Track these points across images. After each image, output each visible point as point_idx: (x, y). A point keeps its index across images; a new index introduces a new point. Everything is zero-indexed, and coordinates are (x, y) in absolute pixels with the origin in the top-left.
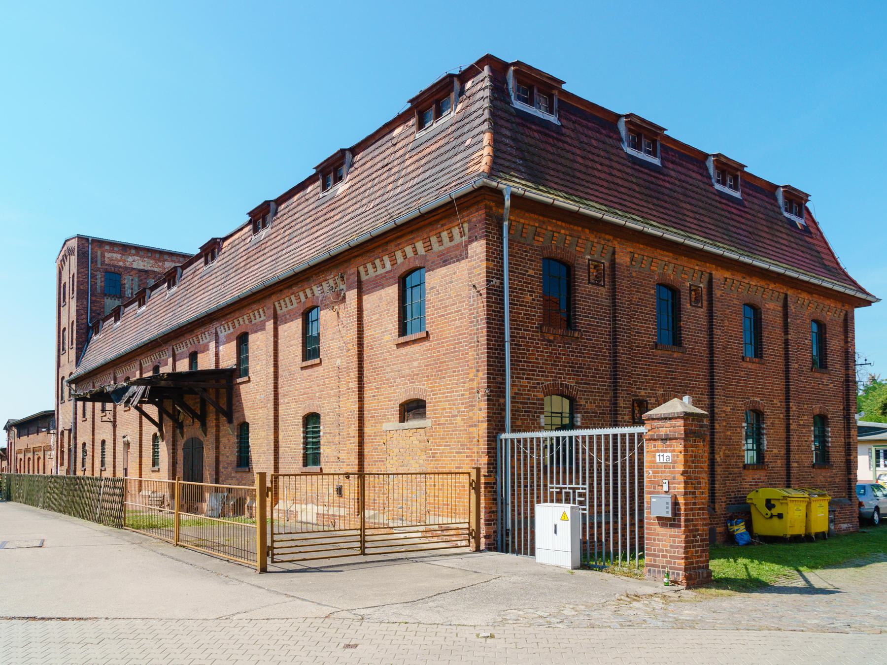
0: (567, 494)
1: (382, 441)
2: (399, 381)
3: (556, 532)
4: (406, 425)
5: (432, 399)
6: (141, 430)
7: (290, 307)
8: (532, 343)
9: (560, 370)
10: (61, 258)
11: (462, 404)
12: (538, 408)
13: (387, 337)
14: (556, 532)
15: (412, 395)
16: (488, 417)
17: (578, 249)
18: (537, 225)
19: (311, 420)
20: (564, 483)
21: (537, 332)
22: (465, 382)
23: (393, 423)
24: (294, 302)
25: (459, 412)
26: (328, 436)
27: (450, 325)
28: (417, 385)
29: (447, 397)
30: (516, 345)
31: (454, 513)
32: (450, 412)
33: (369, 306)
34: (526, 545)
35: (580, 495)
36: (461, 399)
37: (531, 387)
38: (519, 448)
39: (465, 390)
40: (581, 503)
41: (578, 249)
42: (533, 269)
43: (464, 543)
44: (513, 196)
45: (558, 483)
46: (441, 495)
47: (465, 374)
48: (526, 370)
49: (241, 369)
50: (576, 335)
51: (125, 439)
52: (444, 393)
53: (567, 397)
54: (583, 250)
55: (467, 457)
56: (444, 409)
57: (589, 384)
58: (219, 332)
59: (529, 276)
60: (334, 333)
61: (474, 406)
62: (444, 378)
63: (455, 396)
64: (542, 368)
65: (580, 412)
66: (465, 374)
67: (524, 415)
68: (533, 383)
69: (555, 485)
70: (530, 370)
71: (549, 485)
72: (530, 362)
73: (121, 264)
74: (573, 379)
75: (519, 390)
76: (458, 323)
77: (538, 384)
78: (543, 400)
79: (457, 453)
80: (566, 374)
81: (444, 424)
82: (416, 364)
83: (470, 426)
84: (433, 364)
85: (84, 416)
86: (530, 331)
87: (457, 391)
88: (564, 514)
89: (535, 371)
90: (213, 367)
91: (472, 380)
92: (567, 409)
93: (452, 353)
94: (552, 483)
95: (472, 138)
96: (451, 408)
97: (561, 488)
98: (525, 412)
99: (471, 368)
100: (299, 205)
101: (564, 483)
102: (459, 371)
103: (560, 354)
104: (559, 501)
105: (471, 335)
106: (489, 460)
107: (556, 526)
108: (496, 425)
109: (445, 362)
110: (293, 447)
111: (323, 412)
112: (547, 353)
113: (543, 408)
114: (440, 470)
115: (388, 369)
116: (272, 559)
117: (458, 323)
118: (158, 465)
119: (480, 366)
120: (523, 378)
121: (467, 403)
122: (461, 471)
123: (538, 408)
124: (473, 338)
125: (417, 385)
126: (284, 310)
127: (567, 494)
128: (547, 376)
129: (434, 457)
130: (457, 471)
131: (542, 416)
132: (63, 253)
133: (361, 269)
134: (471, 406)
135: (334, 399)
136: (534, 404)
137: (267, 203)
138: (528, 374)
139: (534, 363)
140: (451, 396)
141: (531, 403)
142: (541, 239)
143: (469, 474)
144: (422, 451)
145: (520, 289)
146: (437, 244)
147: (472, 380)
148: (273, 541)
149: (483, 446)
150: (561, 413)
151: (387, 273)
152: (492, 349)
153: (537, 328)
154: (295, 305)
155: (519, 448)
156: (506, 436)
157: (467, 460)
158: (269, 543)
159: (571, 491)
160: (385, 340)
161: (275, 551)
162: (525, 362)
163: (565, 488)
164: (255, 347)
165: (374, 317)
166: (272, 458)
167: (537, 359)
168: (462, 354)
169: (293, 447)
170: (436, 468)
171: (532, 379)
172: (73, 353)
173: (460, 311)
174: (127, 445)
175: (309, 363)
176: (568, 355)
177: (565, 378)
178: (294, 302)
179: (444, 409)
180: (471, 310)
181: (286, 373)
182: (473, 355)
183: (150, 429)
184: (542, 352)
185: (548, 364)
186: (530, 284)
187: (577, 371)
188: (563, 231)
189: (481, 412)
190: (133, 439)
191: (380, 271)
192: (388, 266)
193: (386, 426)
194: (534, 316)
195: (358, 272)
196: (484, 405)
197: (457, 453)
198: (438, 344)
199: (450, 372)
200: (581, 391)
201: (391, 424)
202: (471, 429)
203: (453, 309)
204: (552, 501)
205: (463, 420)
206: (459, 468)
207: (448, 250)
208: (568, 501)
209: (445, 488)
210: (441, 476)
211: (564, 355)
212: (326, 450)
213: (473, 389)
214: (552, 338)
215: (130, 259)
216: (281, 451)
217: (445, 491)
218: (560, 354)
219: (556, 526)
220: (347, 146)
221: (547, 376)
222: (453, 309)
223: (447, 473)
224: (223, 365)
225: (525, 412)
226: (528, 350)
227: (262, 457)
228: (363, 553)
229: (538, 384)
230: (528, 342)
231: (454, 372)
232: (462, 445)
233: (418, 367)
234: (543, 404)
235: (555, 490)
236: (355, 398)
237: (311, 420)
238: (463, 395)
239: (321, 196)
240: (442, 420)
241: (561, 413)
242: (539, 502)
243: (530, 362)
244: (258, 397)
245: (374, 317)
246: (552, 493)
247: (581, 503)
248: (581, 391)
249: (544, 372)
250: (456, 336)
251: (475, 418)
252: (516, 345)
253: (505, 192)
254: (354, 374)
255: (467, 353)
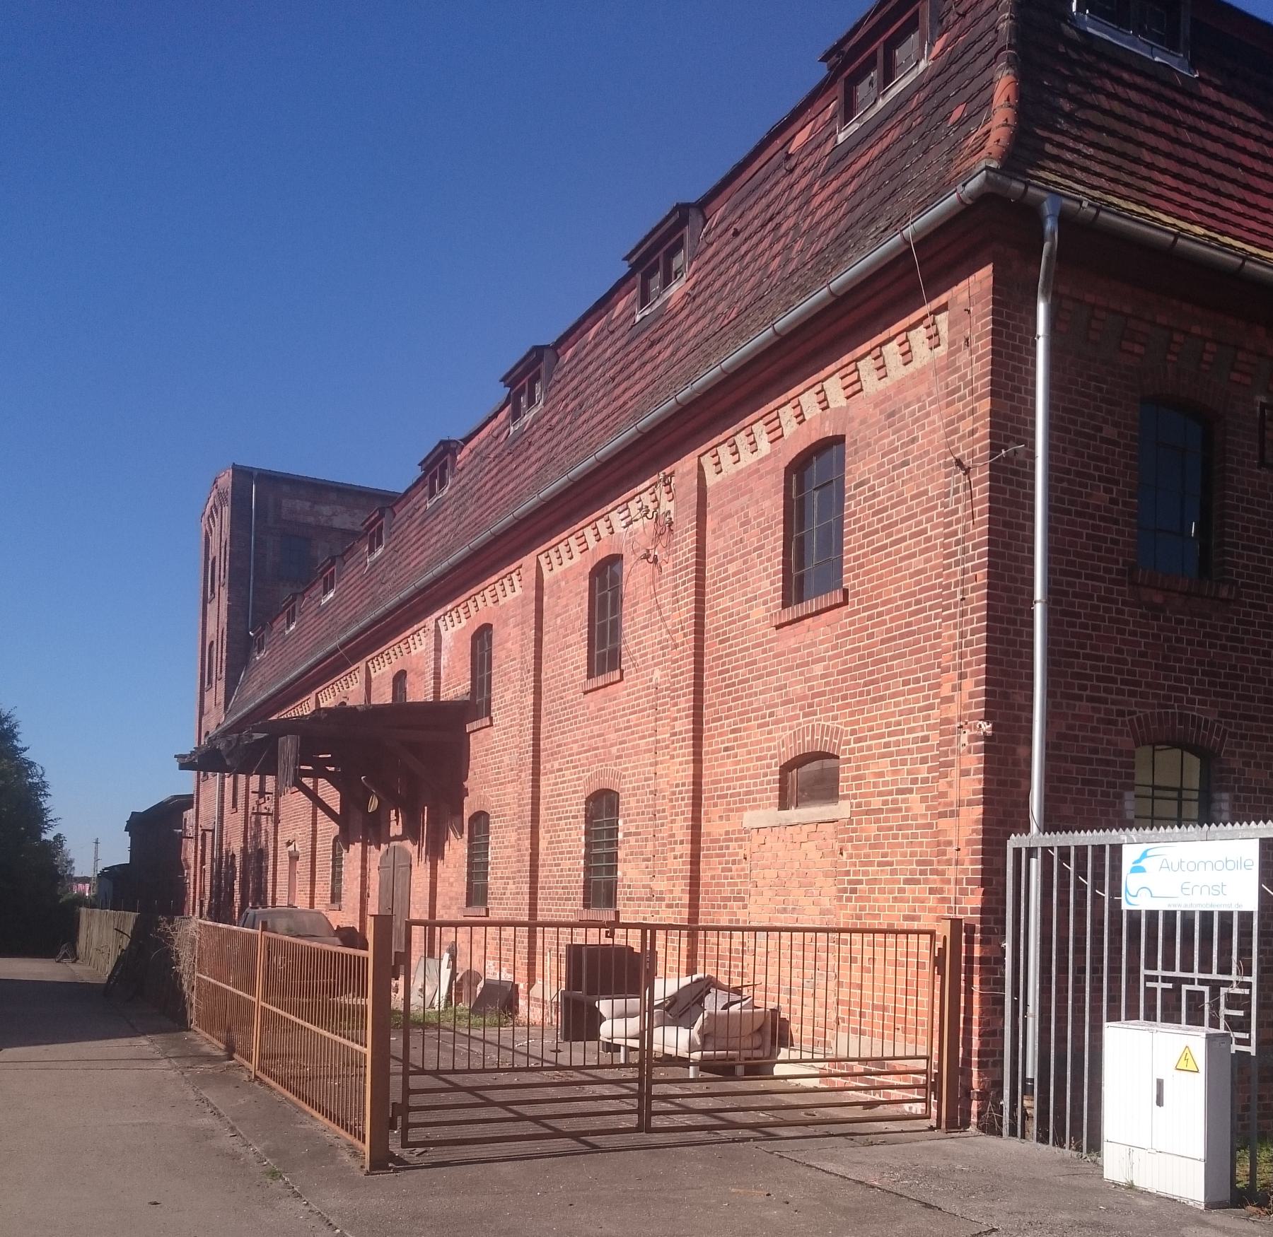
0: (1195, 998)
1: (741, 852)
2: (780, 711)
3: (1160, 1102)
4: (794, 814)
5: (852, 751)
6: (314, 831)
7: (568, 563)
8: (1107, 610)
9: (1178, 679)
10: (208, 512)
11: (924, 760)
12: (1117, 775)
13: (758, 612)
14: (1160, 1102)
15: (806, 744)
16: (985, 791)
17: (1235, 376)
18: (1127, 309)
19: (602, 807)
20: (1187, 967)
21: (1121, 583)
22: (931, 707)
23: (764, 814)
24: (576, 550)
25: (914, 781)
26: (632, 839)
27: (898, 570)
28: (820, 720)
29: (887, 745)
30: (1065, 613)
31: (899, 1025)
32: (894, 782)
33: (721, 543)
34: (1077, 1119)
35: (1233, 1001)
36: (920, 750)
37: (1100, 720)
38: (1064, 874)
39: (930, 727)
40: (1235, 1024)
41: (1235, 376)
42: (1116, 425)
43: (918, 1108)
44: (1065, 219)
45: (1169, 965)
46: (867, 983)
47: (931, 688)
48: (1089, 678)
49: (476, 706)
50: (1224, 593)
51: (291, 848)
52: (882, 736)
53: (1195, 750)
54: (1248, 381)
55: (932, 891)
56: (881, 775)
57: (1253, 718)
58: (443, 629)
59: (1103, 440)
60: (650, 612)
61: (951, 764)
62: (882, 698)
63: (906, 742)
64: (1130, 673)
65: (1227, 790)
66: (931, 688)
67: (1080, 792)
68: (1108, 712)
69: (1159, 972)
70: (1099, 679)
71: (1143, 972)
72: (1101, 659)
73: (311, 519)
74: (1213, 704)
75: (1071, 727)
76: (917, 563)
77: (1121, 713)
78: (1131, 754)
79: (907, 881)
80: (1195, 692)
81: (880, 811)
82: (818, 669)
83: (942, 815)
84: (857, 668)
85: (235, 805)
86: (1102, 579)
87: (911, 731)
88: (1187, 1053)
89: (1114, 681)
90: (430, 698)
91: (949, 700)
92: (1193, 779)
93: (902, 636)
94: (1151, 965)
95: (968, 101)
96: (895, 772)
97: (1178, 982)
98: (1085, 782)
99: (946, 670)
100: (596, 346)
101: (1187, 967)
102: (917, 681)
103: (1179, 640)
104: (1171, 1016)
105: (948, 587)
106: (984, 902)
107: (1160, 1084)
108: (1002, 811)
109: (884, 660)
110: (566, 864)
111: (625, 788)
112: (1145, 635)
113: (1132, 776)
114: (869, 923)
115: (758, 686)
116: (404, 1136)
117: (917, 563)
118: (340, 899)
119: (968, 664)
120: (1080, 698)
121: (934, 758)
122: (915, 925)
123: (1117, 775)
124: (954, 595)
125: (820, 720)
126: (558, 569)
127: (1195, 998)
128: (1143, 695)
129: (854, 891)
130: (906, 925)
131: (1129, 795)
132: (210, 504)
133: (708, 461)
134: (943, 765)
135: (648, 758)
136: (1108, 763)
137: (538, 351)
138: (1094, 688)
139: (1110, 660)
140: (897, 743)
141: (1100, 761)
142: (1137, 349)
143: (932, 933)
144: (826, 875)
145: (1078, 474)
146: (875, 375)
147: (949, 700)
148: (407, 1092)
149: (971, 866)
150: (1180, 790)
151: (761, 461)
152: (1001, 620)
153: (1120, 572)
154: (578, 557)
155: (1064, 874)
156: (1035, 836)
157: (932, 901)
158: (396, 1096)
159: (1206, 989)
160: (753, 619)
161: (414, 1118)
162: (1087, 657)
163: (1192, 981)
164: (503, 654)
165: (732, 568)
166: (526, 888)
167: (1119, 651)
168: (927, 639)
169: (566, 864)
170: (859, 917)
171: (1105, 701)
172: (221, 686)
173: (924, 531)
174: (294, 858)
175: (600, 681)
176: (1201, 644)
177: (1192, 701)
178: (576, 550)
179: (881, 775)
180: (949, 524)
181: (556, 706)
182: (951, 637)
183: (329, 829)
184: (1133, 633)
185: (1148, 665)
186: (1106, 460)
187: (1223, 685)
188: (1196, 330)
189: (967, 784)
190: (302, 847)
191: (747, 459)
192: (764, 447)
193: (751, 818)
194: (1115, 542)
195: (700, 467)
196: (975, 762)
197: (907, 881)
198: (870, 618)
199: (896, 685)
200: (1233, 735)
201: (761, 812)
202: (944, 823)
203: (905, 530)
204: (1150, 1016)
205: (924, 800)
206: (913, 918)
207: (900, 387)
208: (1195, 1019)
209: (879, 965)
210: (868, 937)
211: (1190, 642)
212: (628, 872)
213: (947, 721)
214: (1158, 599)
215: (326, 510)
216: (542, 873)
217: (879, 975)
218: (1179, 640)
219: (1160, 1084)
220: (693, 198)
221: (1143, 695)
222: (905, 530)
223: (884, 932)
224: (447, 694)
225: (1085, 782)
226: (1095, 628)
227: (511, 886)
228: (644, 1127)
229: (1121, 713)
230: (1096, 608)
231: (906, 683)
232: (919, 863)
233: (823, 676)
234: (1132, 766)
235: (1160, 986)
236: (685, 752)
237: (602, 807)
238: (925, 739)
239: (638, 318)
240: (876, 802)
241: (1180, 790)
242: (1115, 1016)
243: (1101, 659)
244: (506, 758)
245: (732, 568)
246: (1151, 993)
247: (1235, 1024)
248: (1233, 735)
249: (1138, 684)
250: (913, 594)
251: (953, 796)
252: (1065, 613)
253: (1047, 208)
254: (686, 702)
255: (938, 636)
